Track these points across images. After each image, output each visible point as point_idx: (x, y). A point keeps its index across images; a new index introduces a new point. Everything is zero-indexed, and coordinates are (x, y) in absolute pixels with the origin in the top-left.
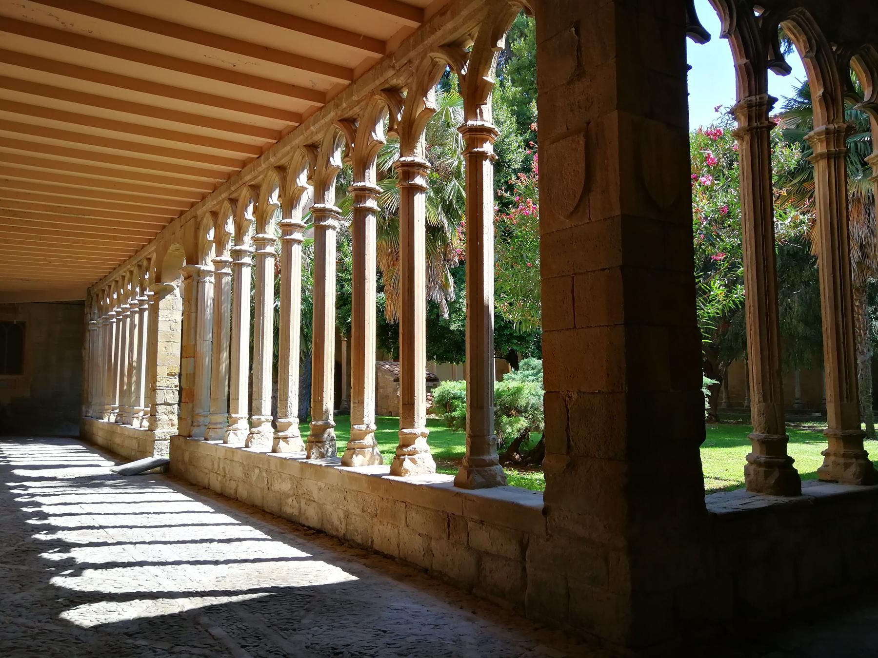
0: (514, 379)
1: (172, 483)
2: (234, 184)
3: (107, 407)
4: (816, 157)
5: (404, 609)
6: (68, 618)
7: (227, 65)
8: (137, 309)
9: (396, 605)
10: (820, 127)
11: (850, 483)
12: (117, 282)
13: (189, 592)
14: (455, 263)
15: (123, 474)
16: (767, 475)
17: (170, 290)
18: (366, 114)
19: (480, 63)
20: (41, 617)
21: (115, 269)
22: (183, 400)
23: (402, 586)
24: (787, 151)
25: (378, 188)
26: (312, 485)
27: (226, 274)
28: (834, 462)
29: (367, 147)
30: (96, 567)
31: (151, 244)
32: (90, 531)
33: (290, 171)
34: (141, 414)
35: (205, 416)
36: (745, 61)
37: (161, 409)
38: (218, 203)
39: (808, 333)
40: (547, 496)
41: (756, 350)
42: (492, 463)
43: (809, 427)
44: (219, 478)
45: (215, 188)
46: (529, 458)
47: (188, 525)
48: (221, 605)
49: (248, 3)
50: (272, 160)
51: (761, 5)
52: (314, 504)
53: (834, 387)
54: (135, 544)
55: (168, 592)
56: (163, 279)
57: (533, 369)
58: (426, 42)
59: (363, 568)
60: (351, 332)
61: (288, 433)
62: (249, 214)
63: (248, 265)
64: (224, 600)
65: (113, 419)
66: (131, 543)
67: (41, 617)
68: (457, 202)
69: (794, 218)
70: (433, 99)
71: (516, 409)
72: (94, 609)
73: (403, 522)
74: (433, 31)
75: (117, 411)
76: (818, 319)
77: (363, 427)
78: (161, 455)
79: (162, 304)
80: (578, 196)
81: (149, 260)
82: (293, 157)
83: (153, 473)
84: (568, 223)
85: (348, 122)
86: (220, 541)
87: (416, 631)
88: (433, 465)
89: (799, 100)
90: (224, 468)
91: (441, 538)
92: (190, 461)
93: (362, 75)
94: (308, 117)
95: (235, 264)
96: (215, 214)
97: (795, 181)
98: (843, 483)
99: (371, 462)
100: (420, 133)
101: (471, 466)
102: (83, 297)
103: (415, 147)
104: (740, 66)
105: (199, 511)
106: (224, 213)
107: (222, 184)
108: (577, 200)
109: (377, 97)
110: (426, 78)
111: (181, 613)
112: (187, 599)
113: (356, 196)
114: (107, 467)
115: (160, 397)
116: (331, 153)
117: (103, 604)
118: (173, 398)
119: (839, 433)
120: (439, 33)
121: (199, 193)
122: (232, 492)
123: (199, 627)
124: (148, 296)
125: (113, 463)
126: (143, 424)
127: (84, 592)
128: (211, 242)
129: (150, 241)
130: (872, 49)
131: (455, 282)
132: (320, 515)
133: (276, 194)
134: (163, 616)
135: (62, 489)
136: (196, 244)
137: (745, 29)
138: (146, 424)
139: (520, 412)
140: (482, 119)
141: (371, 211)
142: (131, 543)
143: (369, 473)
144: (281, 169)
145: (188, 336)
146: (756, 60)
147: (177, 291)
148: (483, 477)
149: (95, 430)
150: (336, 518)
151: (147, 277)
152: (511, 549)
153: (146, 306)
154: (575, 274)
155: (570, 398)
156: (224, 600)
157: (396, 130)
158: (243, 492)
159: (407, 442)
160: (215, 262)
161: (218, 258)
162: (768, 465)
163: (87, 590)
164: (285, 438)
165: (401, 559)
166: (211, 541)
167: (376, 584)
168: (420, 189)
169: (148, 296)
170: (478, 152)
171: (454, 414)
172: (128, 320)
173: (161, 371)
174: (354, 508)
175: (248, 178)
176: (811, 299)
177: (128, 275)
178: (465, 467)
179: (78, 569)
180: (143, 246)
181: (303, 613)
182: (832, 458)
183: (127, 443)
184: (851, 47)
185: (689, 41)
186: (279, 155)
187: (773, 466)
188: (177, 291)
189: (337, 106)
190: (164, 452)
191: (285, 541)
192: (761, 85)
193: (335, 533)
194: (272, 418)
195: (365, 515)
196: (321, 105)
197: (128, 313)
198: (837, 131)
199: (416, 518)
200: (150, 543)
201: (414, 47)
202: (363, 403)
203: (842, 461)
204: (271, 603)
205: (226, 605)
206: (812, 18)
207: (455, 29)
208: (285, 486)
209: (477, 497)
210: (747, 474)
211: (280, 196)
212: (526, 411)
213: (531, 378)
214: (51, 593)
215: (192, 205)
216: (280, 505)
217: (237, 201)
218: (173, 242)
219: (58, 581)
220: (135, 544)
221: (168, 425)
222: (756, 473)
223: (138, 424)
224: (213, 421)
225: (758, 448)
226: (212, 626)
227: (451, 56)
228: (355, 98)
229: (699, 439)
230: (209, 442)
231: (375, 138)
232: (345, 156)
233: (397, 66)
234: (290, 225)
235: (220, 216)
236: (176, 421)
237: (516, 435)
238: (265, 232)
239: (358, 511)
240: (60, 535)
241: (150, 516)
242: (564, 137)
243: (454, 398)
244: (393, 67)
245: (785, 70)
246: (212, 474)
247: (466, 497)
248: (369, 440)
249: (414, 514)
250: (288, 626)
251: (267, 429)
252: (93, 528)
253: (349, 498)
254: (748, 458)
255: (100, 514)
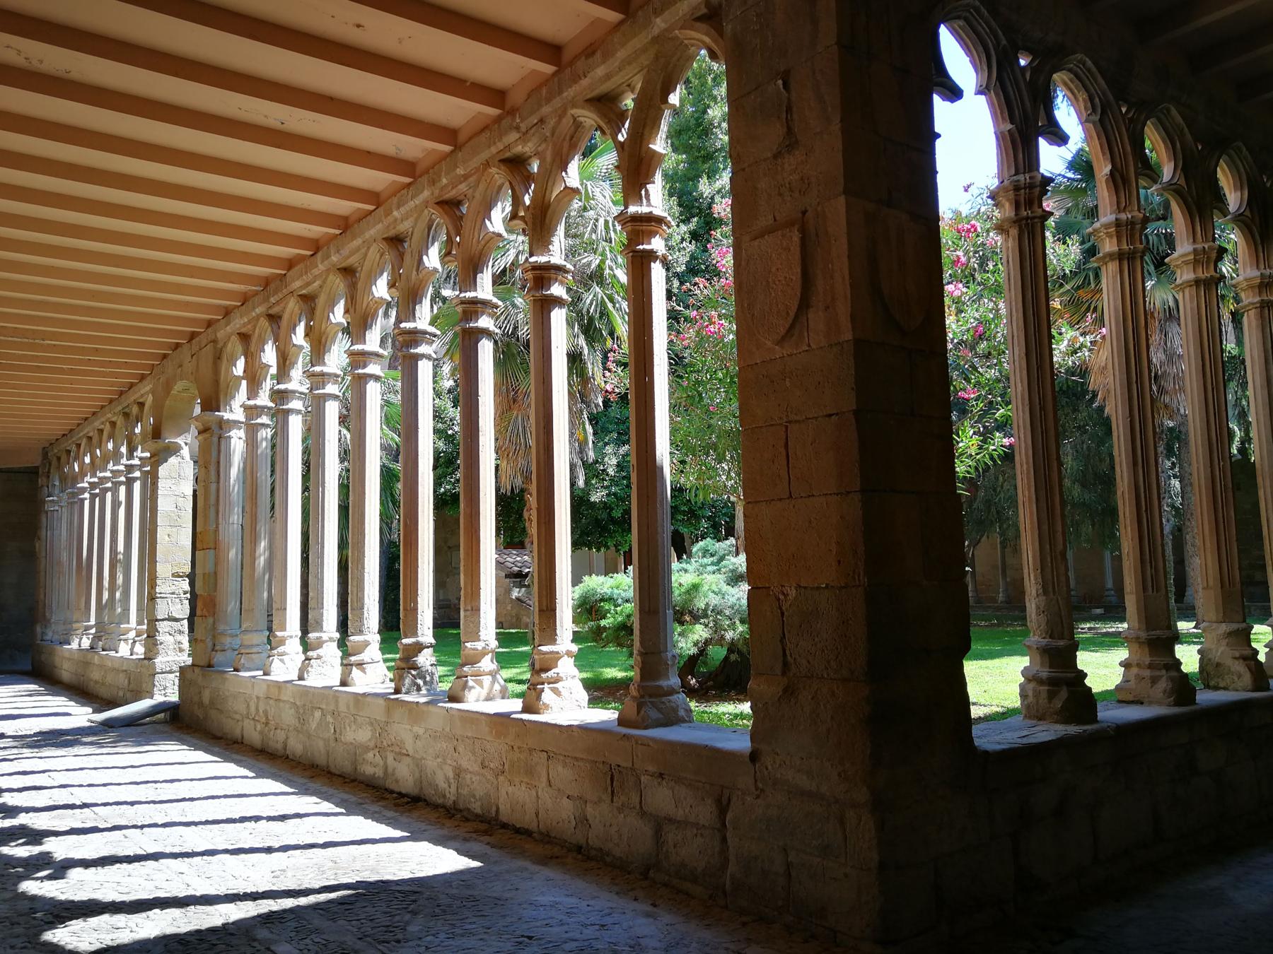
0: (686, 571)
1: (185, 737)
2: (275, 293)
3: (75, 626)
4: (1104, 257)
5: (553, 905)
6: (55, 940)
7: (272, 122)
8: (123, 479)
9: (543, 899)
10: (1107, 217)
11: (1160, 703)
12: (90, 438)
13: (235, 895)
14: (597, 406)
15: (109, 725)
16: (1051, 696)
17: (173, 450)
18: (477, 195)
19: (644, 127)
20: (14, 941)
21: (86, 419)
22: (198, 612)
23: (546, 872)
24: (1060, 249)
25: (495, 300)
26: (404, 732)
27: (263, 425)
28: (1137, 676)
29: (479, 242)
30: (86, 864)
31: (145, 382)
32: (70, 812)
33: (362, 275)
34: (132, 634)
35: (232, 636)
36: (1010, 126)
37: (163, 627)
38: (249, 322)
39: (1087, 497)
40: (755, 734)
41: (1032, 523)
42: (672, 692)
43: (1090, 629)
44: (259, 727)
45: (245, 299)
46: (710, 683)
47: (219, 797)
48: (285, 911)
49: (204, 4)
50: (334, 258)
51: (1029, 50)
52: (408, 760)
53: (1135, 572)
54: (142, 827)
55: (202, 896)
56: (165, 433)
57: (712, 555)
58: (565, 94)
59: (488, 850)
60: (453, 509)
61: (364, 657)
62: (299, 337)
63: (298, 412)
64: (289, 903)
65: (86, 643)
66: (135, 827)
67: (14, 941)
68: (601, 317)
69: (1072, 341)
70: (573, 175)
71: (691, 613)
72: (94, 926)
73: (544, 779)
74: (576, 79)
75: (93, 631)
76: (1108, 481)
77: (479, 645)
78: (165, 695)
79: (163, 470)
80: (792, 314)
81: (141, 405)
82: (366, 255)
83: (154, 722)
84: (779, 352)
85: (450, 206)
86: (270, 819)
87: (578, 936)
88: (584, 696)
89: (1070, 175)
90: (266, 712)
91: (600, 800)
92: (212, 702)
93: (470, 139)
94: (389, 198)
95: (278, 411)
96: (245, 337)
97: (1067, 287)
98: (1150, 703)
99: (489, 698)
100: (558, 222)
101: (642, 697)
102: (34, 460)
103: (550, 243)
104: (1002, 133)
105: (232, 776)
106: (260, 336)
107: (256, 293)
108: (790, 320)
109: (493, 170)
110: (566, 144)
111: (225, 926)
112: (232, 905)
113: (464, 312)
114: (81, 716)
115: (162, 610)
116: (424, 250)
117: (105, 918)
118: (181, 609)
119: (1143, 635)
120: (585, 82)
121: (219, 306)
122: (280, 746)
123: (255, 944)
124: (141, 459)
125: (90, 710)
126: (135, 650)
127: (73, 902)
128: (239, 379)
129: (142, 378)
130: (1174, 112)
131: (594, 434)
132: (417, 775)
133: (339, 309)
134: (198, 932)
135: (15, 751)
136: (217, 382)
137: (1008, 84)
138: (140, 650)
139: (696, 618)
140: (649, 204)
141: (485, 333)
142: (135, 827)
143: (492, 712)
144: (348, 272)
145: (206, 516)
146: (1024, 125)
147: (185, 452)
148: (659, 710)
149: (57, 661)
150: (442, 779)
151: (138, 430)
152: (705, 813)
153: (137, 474)
154: (790, 422)
155: (786, 595)
156: (333, 895)
157: (523, 218)
158: (296, 746)
159: (541, 667)
160: (247, 408)
161: (251, 403)
162: (1053, 683)
163: (77, 898)
164: (360, 665)
165: (541, 833)
166: (257, 819)
167: (508, 872)
168: (558, 302)
169: (141, 459)
170: (644, 251)
171: (603, 623)
172: (109, 495)
173: (163, 570)
174: (468, 762)
175: (297, 284)
176: (1089, 448)
177: (107, 428)
178: (633, 697)
179: (61, 869)
180: (132, 385)
181: (408, 917)
182: (1135, 670)
183: (109, 679)
184: (1145, 109)
185: (937, 99)
186: (345, 252)
187: (1058, 683)
188: (185, 452)
189: (433, 182)
190: (169, 691)
191: (367, 815)
192: (1032, 160)
193: (440, 801)
194: (338, 635)
195: (484, 771)
196: (407, 180)
197: (109, 485)
198: (1131, 223)
199: (562, 773)
200: (165, 825)
201: (548, 100)
202: (478, 610)
203: (1147, 673)
204: (359, 905)
205: (291, 910)
206: (1094, 69)
207: (608, 77)
208: (362, 735)
209: (653, 740)
210: (1023, 695)
211: (347, 311)
212: (706, 616)
213: (710, 568)
214: (26, 905)
215: (210, 324)
216: (354, 763)
217: (280, 317)
218: (179, 378)
219: (30, 887)
220: (142, 827)
221: (175, 651)
222: (1037, 694)
223: (128, 649)
224: (246, 643)
225: (1038, 658)
226: (276, 942)
227: (603, 115)
228: (460, 171)
229: (962, 650)
230: (241, 674)
231: (491, 229)
232: (446, 255)
233: (523, 127)
234: (363, 354)
235: (254, 340)
236: (186, 645)
237: (694, 651)
238: (324, 364)
239: (476, 768)
240: (23, 819)
241: (158, 785)
242: (769, 231)
243: (602, 600)
244: (517, 128)
245: (1060, 138)
246: (246, 722)
247: (637, 740)
248: (487, 664)
249: (560, 768)
250: (388, 936)
251: (331, 652)
252: (72, 807)
253: (460, 749)
254: (1023, 673)
255: (81, 786)
